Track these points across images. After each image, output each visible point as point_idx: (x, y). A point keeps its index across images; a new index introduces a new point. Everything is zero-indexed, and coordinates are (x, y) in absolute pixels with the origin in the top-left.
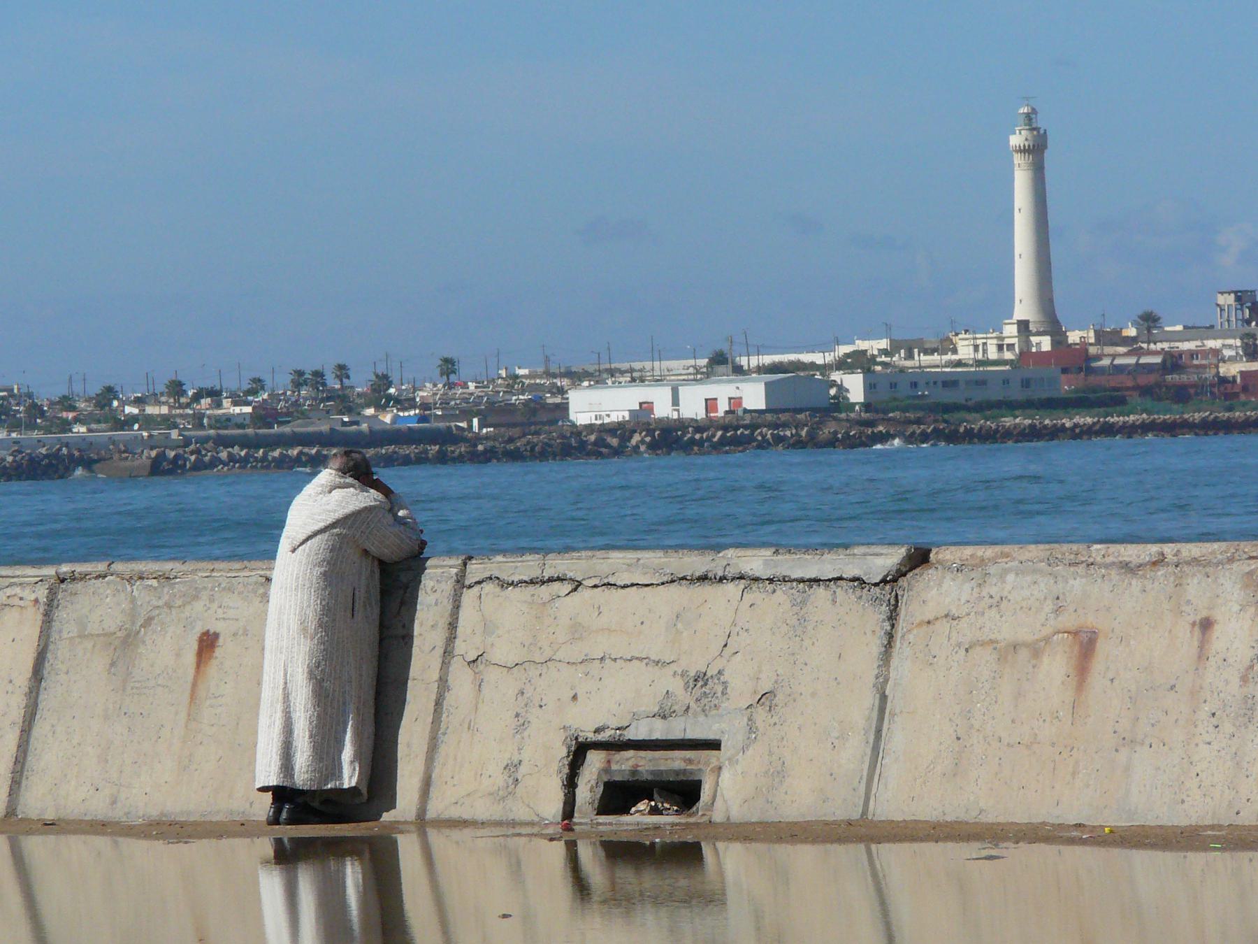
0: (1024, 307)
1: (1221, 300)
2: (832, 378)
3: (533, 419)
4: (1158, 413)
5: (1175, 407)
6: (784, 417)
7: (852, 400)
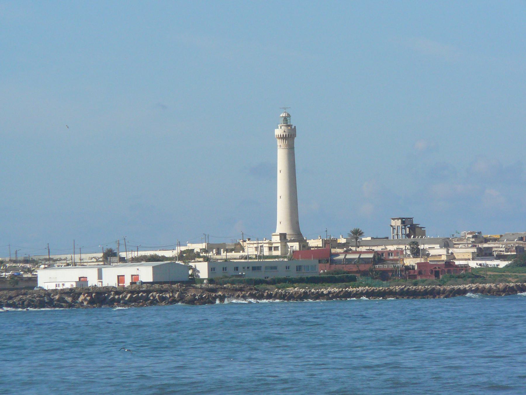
0: (282, 226)
1: (393, 223)
2: (191, 264)
3: (17, 286)
4: (375, 286)
5: (385, 282)
6: (165, 286)
7: (201, 277)
